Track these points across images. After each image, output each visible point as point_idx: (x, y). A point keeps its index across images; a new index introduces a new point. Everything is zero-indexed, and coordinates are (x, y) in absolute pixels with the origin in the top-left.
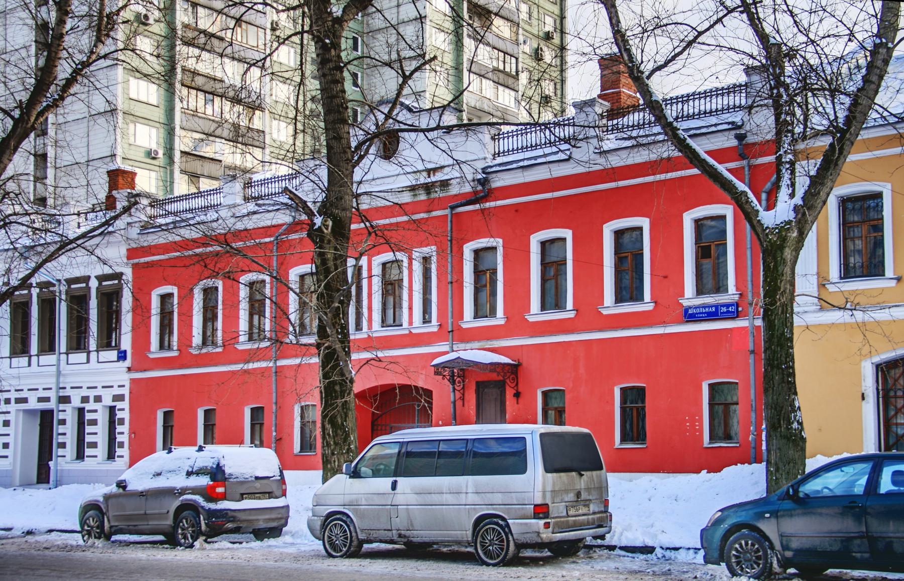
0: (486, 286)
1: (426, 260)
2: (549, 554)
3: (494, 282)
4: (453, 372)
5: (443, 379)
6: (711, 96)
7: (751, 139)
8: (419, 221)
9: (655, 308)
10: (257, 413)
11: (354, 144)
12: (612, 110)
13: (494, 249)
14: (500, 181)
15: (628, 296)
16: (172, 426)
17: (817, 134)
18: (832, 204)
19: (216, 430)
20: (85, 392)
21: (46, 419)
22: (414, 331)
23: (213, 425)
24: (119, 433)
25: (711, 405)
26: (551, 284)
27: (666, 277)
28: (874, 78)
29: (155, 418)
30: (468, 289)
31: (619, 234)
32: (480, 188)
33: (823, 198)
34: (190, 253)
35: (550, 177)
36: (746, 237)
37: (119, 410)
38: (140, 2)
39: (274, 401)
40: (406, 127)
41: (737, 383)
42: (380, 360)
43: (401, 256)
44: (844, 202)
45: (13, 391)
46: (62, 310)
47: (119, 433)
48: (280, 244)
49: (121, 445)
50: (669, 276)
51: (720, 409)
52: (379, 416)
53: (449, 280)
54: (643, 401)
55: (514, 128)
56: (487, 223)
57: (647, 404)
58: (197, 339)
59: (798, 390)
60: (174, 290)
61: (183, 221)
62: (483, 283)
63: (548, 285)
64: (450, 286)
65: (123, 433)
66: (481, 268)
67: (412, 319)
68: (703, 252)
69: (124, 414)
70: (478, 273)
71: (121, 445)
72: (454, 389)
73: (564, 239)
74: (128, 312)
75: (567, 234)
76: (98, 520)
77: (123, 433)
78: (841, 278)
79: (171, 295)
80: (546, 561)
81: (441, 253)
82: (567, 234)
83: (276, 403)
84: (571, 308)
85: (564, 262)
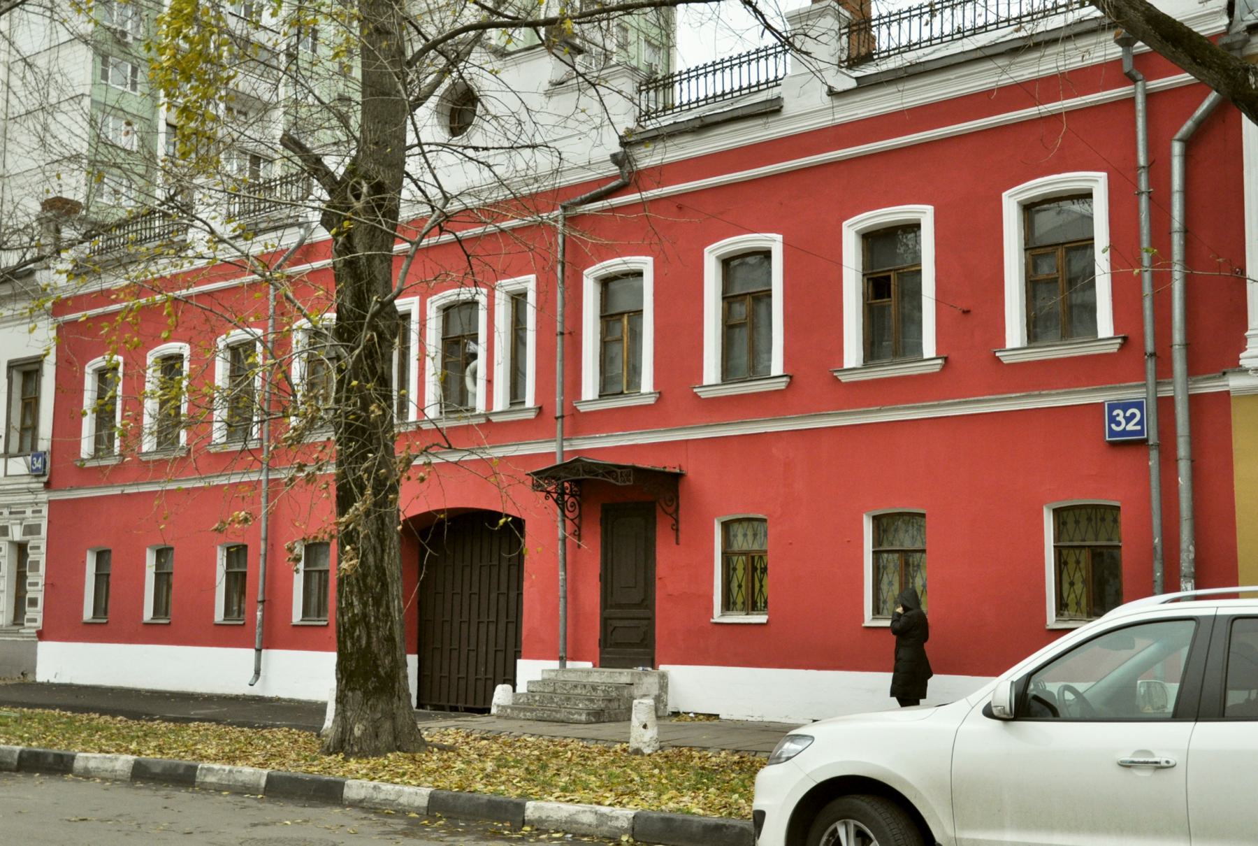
0: (620, 340)
1: (518, 300)
2: (1185, 78)
3: (636, 335)
4: (563, 489)
5: (546, 498)
9: (789, 385)
10: (237, 554)
11: (409, 54)
13: (639, 274)
14: (648, 158)
16: (108, 575)
19: (173, 579)
22: (495, 419)
23: (169, 574)
24: (31, 584)
25: (877, 554)
26: (741, 336)
27: (966, 312)
28: (326, 180)
29: (84, 562)
30: (433, 332)
31: (871, 239)
34: (474, 457)
36: (563, 359)
37: (32, 548)
38: (65, 9)
39: (263, 535)
40: (501, 19)
42: (502, 231)
47: (31, 584)
49: (33, 602)
50: (972, 306)
51: (315, 577)
52: (317, 729)
53: (559, 329)
58: (87, 447)
60: (186, 350)
62: (617, 335)
63: (615, 349)
64: (559, 338)
65: (36, 584)
67: (489, 391)
68: (878, 287)
69: (39, 556)
70: (608, 318)
71: (33, 602)
74: (1104, 251)
76: (439, 807)
77: (36, 584)
79: (180, 357)
80: (339, 637)
82: (775, 242)
83: (266, 539)
84: (1110, 333)
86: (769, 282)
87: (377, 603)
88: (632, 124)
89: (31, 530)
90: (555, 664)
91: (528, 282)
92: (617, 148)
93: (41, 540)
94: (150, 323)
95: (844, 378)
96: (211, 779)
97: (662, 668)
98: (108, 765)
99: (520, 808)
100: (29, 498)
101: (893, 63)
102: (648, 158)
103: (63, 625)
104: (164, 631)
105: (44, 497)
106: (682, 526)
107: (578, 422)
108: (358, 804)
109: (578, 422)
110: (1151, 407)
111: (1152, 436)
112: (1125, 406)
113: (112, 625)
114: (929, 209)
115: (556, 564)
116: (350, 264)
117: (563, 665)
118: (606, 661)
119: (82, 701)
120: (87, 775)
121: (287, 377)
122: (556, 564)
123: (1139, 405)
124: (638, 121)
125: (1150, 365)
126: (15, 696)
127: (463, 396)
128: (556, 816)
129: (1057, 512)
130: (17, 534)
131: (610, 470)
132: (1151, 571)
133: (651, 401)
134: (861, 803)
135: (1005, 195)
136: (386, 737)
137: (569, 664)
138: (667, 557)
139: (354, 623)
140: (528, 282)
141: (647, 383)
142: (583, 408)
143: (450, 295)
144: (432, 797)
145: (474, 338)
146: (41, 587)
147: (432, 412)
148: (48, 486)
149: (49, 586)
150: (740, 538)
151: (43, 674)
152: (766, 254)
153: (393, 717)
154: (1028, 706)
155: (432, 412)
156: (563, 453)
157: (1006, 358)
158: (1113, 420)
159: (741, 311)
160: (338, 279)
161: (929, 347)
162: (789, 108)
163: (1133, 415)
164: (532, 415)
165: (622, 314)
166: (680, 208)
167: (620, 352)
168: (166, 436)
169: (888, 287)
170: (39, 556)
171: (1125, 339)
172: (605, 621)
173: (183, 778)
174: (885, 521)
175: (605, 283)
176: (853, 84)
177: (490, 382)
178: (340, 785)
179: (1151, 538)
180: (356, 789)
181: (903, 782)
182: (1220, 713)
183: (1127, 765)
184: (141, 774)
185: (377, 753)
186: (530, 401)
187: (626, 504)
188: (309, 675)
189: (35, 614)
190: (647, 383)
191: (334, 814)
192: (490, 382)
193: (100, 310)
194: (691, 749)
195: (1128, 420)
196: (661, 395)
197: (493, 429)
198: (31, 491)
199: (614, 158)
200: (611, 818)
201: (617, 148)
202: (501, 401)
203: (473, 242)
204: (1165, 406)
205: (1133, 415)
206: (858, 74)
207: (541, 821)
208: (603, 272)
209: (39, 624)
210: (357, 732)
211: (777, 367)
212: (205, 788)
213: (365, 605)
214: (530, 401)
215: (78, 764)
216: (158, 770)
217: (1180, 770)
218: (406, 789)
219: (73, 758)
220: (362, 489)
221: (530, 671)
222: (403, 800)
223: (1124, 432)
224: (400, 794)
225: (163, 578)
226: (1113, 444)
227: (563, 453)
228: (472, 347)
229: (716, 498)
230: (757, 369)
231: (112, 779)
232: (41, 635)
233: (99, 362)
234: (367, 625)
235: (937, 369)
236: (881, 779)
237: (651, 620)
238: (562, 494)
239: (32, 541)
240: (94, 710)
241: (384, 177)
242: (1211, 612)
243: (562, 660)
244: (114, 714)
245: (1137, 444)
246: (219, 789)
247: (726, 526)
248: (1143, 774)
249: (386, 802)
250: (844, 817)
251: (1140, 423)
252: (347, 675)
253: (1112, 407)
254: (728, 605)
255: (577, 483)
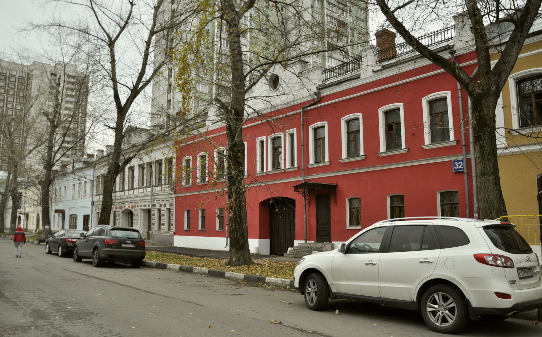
0: (320, 146)
1: (292, 136)
6: (431, 36)
7: (458, 53)
8: (190, 145)
9: (365, 158)
12: (381, 50)
13: (324, 127)
14: (326, 93)
15: (363, 25)
17: (512, 10)
18: (511, 83)
20: (134, 204)
21: (149, 211)
22: (287, 171)
25: (442, 205)
26: (353, 144)
27: (414, 134)
31: (315, 130)
32: (315, 97)
33: (511, 65)
35: (497, 126)
41: (457, 192)
43: (281, 134)
44: (519, 82)
45: (171, 96)
46: (386, 63)
48: (305, 112)
49: (172, 225)
54: (403, 203)
55: (99, 13)
56: (320, 114)
57: (405, 205)
59: (507, 209)
61: (188, 166)
66: (318, 137)
69: (173, 212)
70: (316, 140)
72: (305, 199)
73: (358, 119)
74: (10, 208)
75: (360, 116)
78: (520, 127)
79: (205, 156)
81: (298, 132)
82: (360, 116)
85: (358, 131)
86: (359, 128)
87: (239, 225)
88: (321, 83)
89: (171, 205)
90: (303, 242)
91: (294, 131)
92: (315, 90)
93: (173, 208)
94: (200, 146)
95: (381, 155)
96: (196, 271)
97: (333, 242)
98: (174, 267)
99: (264, 279)
100: (170, 196)
101: (403, 57)
102: (326, 93)
103: (180, 232)
104: (203, 233)
105: (174, 196)
106: (337, 200)
107: (310, 171)
108: (228, 278)
109: (310, 171)
110: (465, 161)
111: (465, 170)
112: (458, 161)
113: (191, 231)
114: (402, 104)
115: (304, 213)
116: (230, 132)
117: (306, 242)
118: (317, 241)
119: (179, 251)
120: (170, 269)
121: (14, 203)
122: (304, 213)
123: (462, 161)
124: (323, 82)
125: (464, 148)
126: (167, 250)
127: (279, 164)
128: (272, 281)
129: (442, 194)
130: (168, 206)
131: (315, 185)
132: (466, 211)
133: (328, 164)
134: (314, 275)
135: (423, 99)
136: (241, 261)
137: (308, 242)
138: (334, 210)
139: (233, 230)
140: (294, 131)
141: (327, 159)
142: (310, 167)
143: (273, 135)
144: (245, 276)
145: (281, 147)
146: (174, 221)
147: (287, 167)
148: (175, 193)
149: (176, 220)
150: (355, 204)
151: (176, 245)
152: (445, 99)
153: (244, 256)
154: (347, 250)
155: (270, 169)
156: (304, 180)
157: (425, 148)
158: (455, 165)
159: (437, 120)
160: (228, 136)
161: (404, 146)
162: (362, 76)
163: (460, 164)
164: (296, 169)
165: (320, 139)
166: (334, 107)
167: (320, 150)
168: (203, 179)
169: (392, 128)
170: (173, 212)
171: (458, 141)
172: (317, 229)
173: (190, 271)
174: (446, 195)
175: (348, 122)
176: (380, 68)
177: (285, 160)
178: (224, 273)
179: (466, 201)
180: (228, 274)
181: (322, 270)
182: (388, 251)
183: (367, 264)
184: (181, 269)
185: (239, 265)
186: (296, 165)
187: (322, 195)
188: (221, 244)
189: (173, 228)
190: (327, 159)
191: (221, 280)
192: (285, 160)
193: (394, 84)
194: (33, 243)
195: (459, 165)
196: (330, 162)
197: (286, 174)
198: (171, 194)
199: (315, 94)
200: (285, 282)
201: (315, 90)
202: (288, 166)
203: (273, 121)
204: (469, 161)
205: (460, 164)
206: (382, 65)
207: (269, 283)
208: (428, 99)
209: (174, 231)
210: (234, 260)
211: (362, 153)
212: (195, 273)
213: (236, 225)
214: (296, 165)
215: (168, 267)
216: (184, 268)
217: (377, 265)
218: (239, 274)
219: (167, 265)
220: (232, 195)
221: (297, 243)
222: (238, 277)
223: (458, 169)
224: (237, 275)
225: (203, 218)
226: (455, 172)
227: (304, 180)
228: (280, 150)
229: (347, 192)
230: (357, 154)
231: (175, 271)
232: (175, 234)
233: (202, 153)
234: (237, 231)
235: (406, 152)
236: (448, 280)
237: (330, 228)
238: (304, 192)
239: (172, 208)
240: (182, 254)
241: (239, 107)
242: (390, 225)
243: (306, 240)
244: (186, 255)
245: (460, 173)
246: (197, 273)
247: (350, 200)
248: (370, 266)
249: (235, 277)
250: (437, 291)
251: (462, 166)
252: (232, 244)
253: (455, 162)
254: (351, 224)
255: (309, 189)
